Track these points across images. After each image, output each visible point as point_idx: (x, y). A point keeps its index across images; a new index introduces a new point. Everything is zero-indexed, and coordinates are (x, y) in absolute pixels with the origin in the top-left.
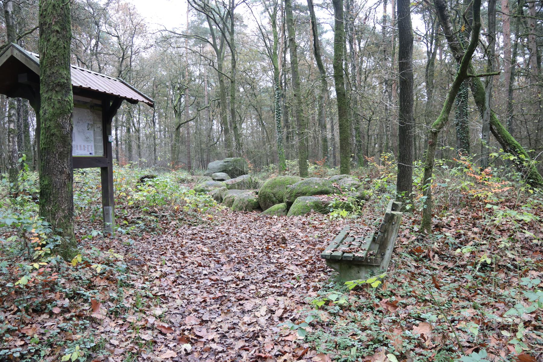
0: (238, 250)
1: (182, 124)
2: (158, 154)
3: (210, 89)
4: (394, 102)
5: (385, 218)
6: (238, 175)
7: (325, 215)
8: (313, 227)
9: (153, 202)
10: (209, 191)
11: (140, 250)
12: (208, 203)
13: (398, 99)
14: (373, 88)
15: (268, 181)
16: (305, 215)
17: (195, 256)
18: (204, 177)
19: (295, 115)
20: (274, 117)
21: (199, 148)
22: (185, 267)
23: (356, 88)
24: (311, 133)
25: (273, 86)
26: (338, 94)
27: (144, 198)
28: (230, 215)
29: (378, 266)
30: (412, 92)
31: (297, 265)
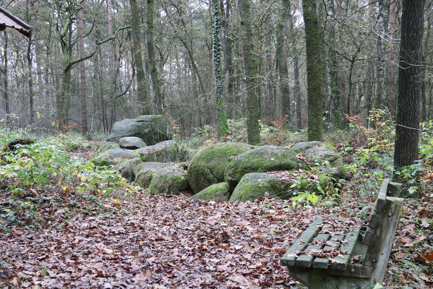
0: (158, 252)
1: (74, 63)
2: (37, 107)
3: (116, 11)
4: (392, 31)
5: (377, 207)
6: (158, 141)
7: (286, 201)
8: (268, 218)
9: (30, 179)
10: (115, 164)
11: (7, 253)
12: (113, 181)
13: (398, 28)
14: (359, 11)
15: (201, 150)
16: (256, 200)
17: (94, 260)
18: (107, 143)
19: (242, 52)
20: (211, 55)
21: (100, 100)
22: (78, 278)
23: (334, 12)
24: (265, 80)
25: (209, 9)
26: (306, 20)
27: (16, 174)
28: (146, 199)
29: (368, 279)
30: (422, 16)
31: (245, 275)
